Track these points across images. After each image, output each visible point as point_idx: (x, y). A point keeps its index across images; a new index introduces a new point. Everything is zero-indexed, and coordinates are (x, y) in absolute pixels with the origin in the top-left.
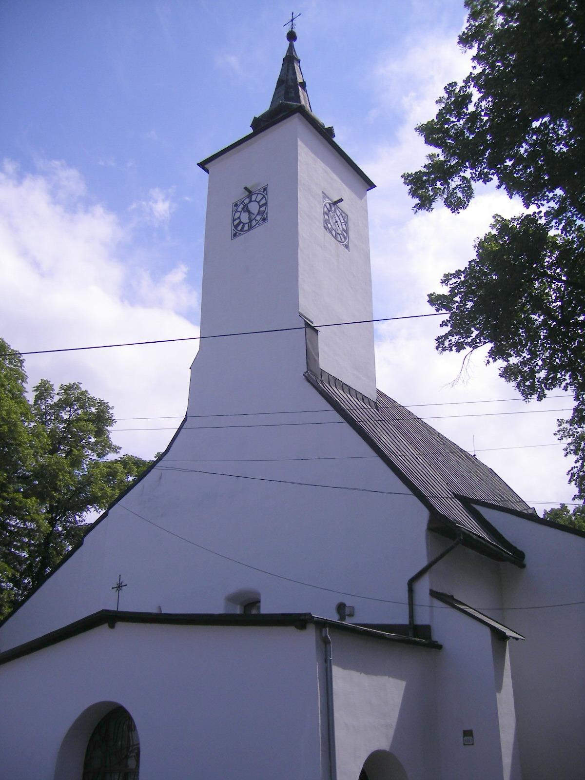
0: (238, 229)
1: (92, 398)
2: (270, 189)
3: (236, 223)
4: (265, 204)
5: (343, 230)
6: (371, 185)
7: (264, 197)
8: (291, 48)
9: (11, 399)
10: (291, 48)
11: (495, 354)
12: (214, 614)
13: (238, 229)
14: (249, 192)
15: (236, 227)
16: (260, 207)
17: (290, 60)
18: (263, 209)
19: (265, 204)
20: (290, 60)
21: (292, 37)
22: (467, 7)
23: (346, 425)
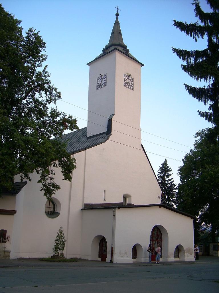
0: (99, 86)
1: (181, 181)
2: (107, 76)
3: (98, 85)
4: (106, 80)
5: (132, 84)
6: (143, 65)
7: (106, 78)
8: (117, 19)
9: (217, 169)
10: (117, 19)
11: (28, 175)
12: (89, 204)
13: (99, 86)
14: (102, 76)
15: (98, 86)
16: (105, 81)
17: (117, 24)
18: (105, 81)
19: (106, 80)
20: (117, 24)
21: (117, 15)
22: (74, 169)
23: (145, 151)
